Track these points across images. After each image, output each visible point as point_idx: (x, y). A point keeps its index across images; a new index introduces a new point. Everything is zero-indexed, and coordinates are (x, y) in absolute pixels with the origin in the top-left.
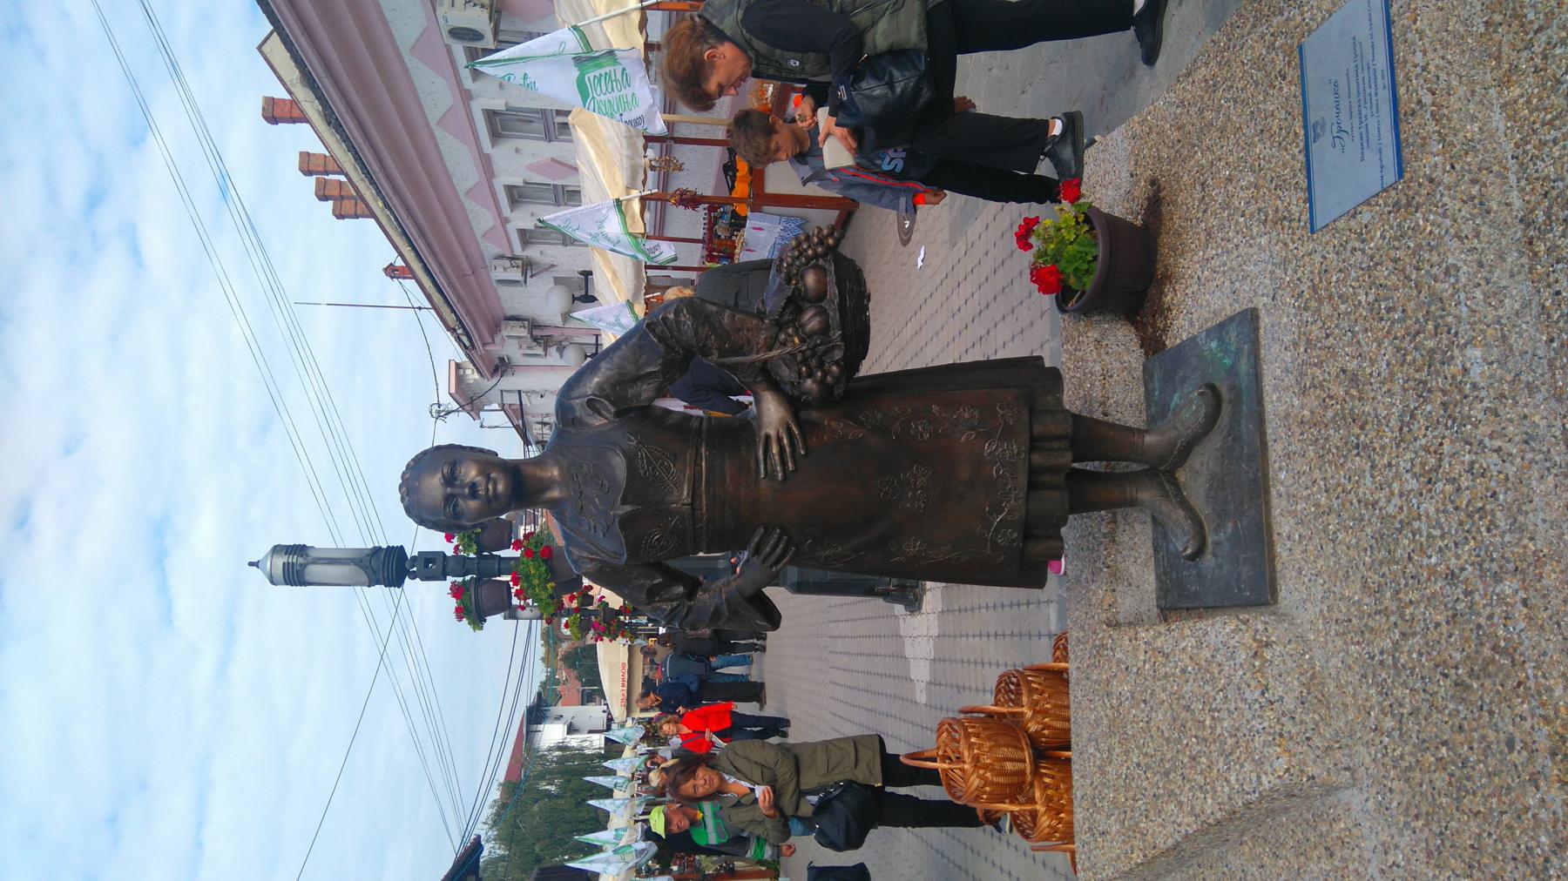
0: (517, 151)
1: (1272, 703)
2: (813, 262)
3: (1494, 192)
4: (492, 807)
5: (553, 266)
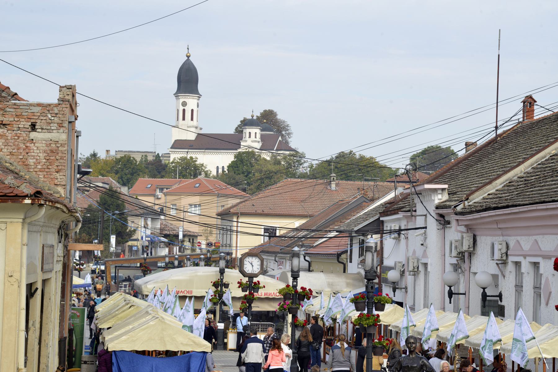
5: (504, 277)
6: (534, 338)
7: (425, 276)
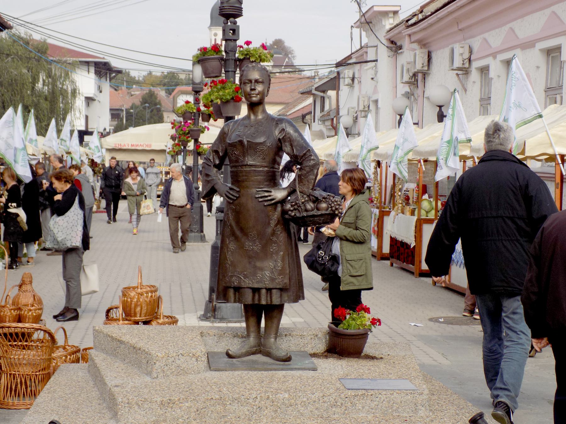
0: (538, 67)
1: (178, 356)
2: (330, 206)
3: (338, 410)
4: (26, 33)
5: (466, 90)
6: (541, 116)
7: (376, 116)
